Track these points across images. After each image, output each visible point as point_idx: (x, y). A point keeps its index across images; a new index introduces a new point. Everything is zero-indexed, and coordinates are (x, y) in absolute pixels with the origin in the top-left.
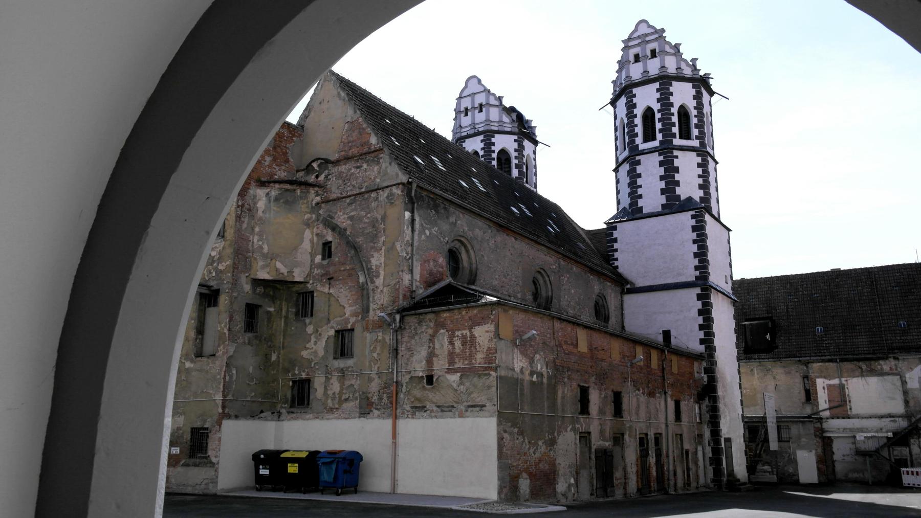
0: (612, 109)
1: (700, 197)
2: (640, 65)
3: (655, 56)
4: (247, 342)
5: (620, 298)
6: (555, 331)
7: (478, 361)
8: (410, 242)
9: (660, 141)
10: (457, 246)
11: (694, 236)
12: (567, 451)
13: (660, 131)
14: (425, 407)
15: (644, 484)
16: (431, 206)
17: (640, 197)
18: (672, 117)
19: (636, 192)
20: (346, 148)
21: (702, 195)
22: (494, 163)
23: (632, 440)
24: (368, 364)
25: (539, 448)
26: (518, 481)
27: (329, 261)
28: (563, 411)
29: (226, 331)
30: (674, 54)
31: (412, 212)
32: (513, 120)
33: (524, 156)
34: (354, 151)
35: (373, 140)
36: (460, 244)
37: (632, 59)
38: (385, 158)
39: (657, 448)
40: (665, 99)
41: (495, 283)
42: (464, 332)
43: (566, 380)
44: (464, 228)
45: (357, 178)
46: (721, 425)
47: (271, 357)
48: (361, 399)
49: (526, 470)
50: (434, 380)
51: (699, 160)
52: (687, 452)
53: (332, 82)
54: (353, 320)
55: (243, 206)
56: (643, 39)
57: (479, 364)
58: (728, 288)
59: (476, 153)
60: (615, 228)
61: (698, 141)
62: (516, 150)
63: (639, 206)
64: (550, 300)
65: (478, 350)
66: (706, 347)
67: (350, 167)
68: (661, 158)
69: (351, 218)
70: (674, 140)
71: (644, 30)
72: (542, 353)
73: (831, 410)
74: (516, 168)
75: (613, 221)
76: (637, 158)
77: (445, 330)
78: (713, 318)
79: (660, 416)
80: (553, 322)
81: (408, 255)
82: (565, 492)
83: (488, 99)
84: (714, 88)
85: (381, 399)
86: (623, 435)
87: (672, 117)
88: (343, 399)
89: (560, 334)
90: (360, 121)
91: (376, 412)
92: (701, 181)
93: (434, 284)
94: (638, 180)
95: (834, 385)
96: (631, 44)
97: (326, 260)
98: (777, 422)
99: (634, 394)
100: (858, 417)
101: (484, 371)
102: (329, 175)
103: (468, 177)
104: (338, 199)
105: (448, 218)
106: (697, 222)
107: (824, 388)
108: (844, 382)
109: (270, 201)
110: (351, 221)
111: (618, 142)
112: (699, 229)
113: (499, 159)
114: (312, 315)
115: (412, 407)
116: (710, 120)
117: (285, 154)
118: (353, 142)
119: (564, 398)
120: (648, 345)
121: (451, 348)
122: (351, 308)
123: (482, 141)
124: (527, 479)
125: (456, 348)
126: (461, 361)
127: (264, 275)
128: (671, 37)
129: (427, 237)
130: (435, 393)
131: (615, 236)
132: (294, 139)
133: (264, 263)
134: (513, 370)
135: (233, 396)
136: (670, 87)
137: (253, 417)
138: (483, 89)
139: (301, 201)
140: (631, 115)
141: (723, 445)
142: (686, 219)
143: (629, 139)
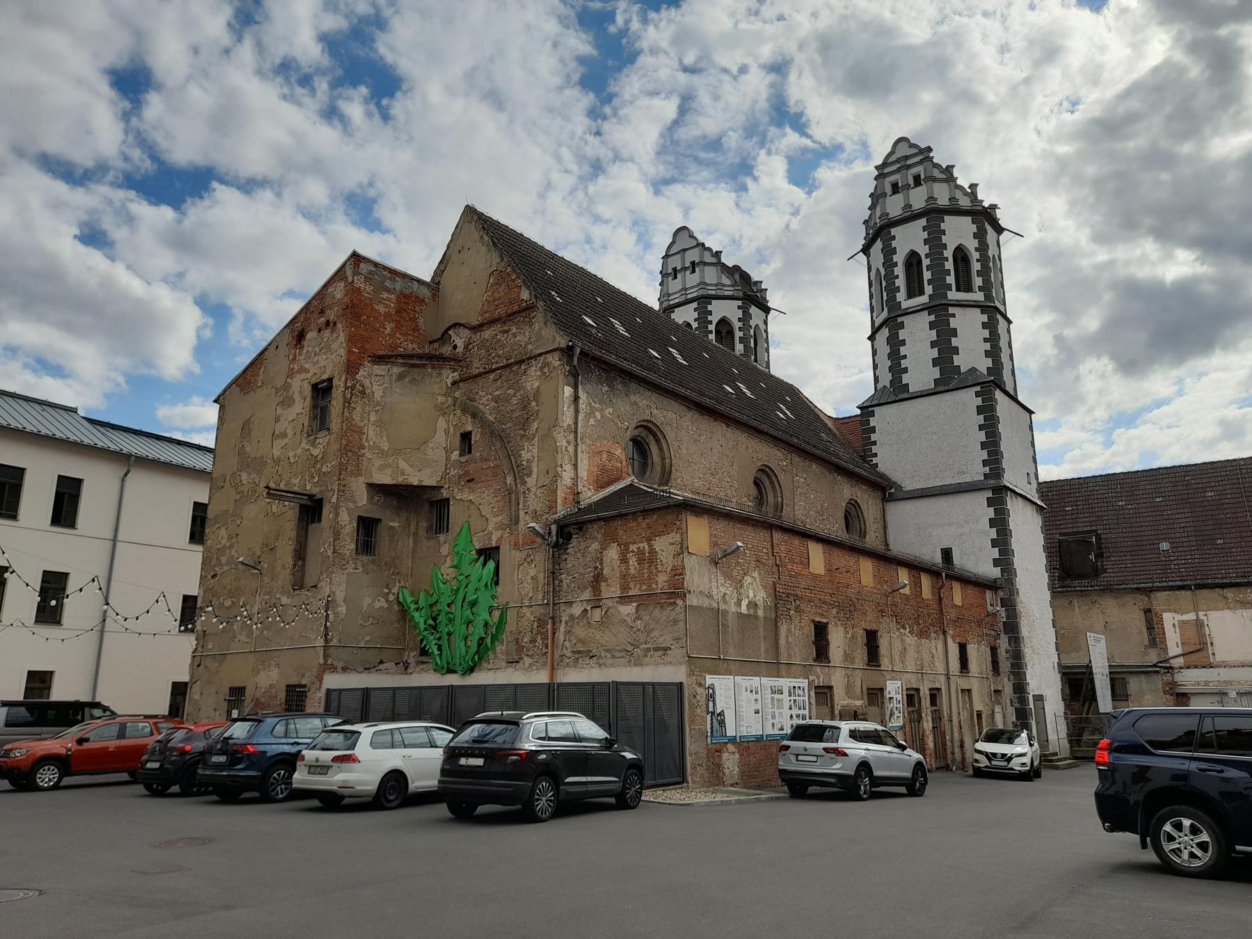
0: (866, 258)
3: (920, 184)
7: (660, 586)
10: (643, 435)
13: (930, 282)
14: (591, 651)
17: (905, 370)
22: (712, 337)
26: (720, 757)
28: (789, 656)
31: (576, 388)
34: (502, 311)
35: (525, 295)
36: (646, 432)
37: (888, 190)
38: (539, 317)
40: (935, 240)
42: (641, 545)
43: (792, 612)
45: (503, 346)
51: (985, 318)
52: (979, 715)
54: (499, 533)
55: (353, 388)
56: (903, 163)
57: (661, 589)
59: (689, 325)
60: (872, 414)
64: (780, 508)
68: (932, 318)
69: (496, 400)
71: (904, 150)
73: (1186, 657)
76: (899, 320)
79: (937, 664)
83: (702, 256)
84: (1002, 223)
91: (527, 661)
92: (988, 346)
93: (609, 484)
94: (902, 348)
95: (1188, 622)
96: (886, 171)
98: (1110, 673)
100: (1224, 665)
101: (668, 599)
103: (662, 346)
104: (480, 375)
107: (1174, 625)
108: (1201, 617)
111: (873, 301)
112: (987, 410)
113: (718, 332)
114: (447, 531)
115: (573, 652)
116: (999, 266)
120: (916, 567)
122: (494, 520)
124: (734, 753)
126: (638, 586)
127: (385, 479)
128: (939, 157)
130: (604, 632)
136: (942, 224)
137: (369, 669)
138: (695, 243)
140: (889, 264)
141: (1032, 706)
142: (969, 399)
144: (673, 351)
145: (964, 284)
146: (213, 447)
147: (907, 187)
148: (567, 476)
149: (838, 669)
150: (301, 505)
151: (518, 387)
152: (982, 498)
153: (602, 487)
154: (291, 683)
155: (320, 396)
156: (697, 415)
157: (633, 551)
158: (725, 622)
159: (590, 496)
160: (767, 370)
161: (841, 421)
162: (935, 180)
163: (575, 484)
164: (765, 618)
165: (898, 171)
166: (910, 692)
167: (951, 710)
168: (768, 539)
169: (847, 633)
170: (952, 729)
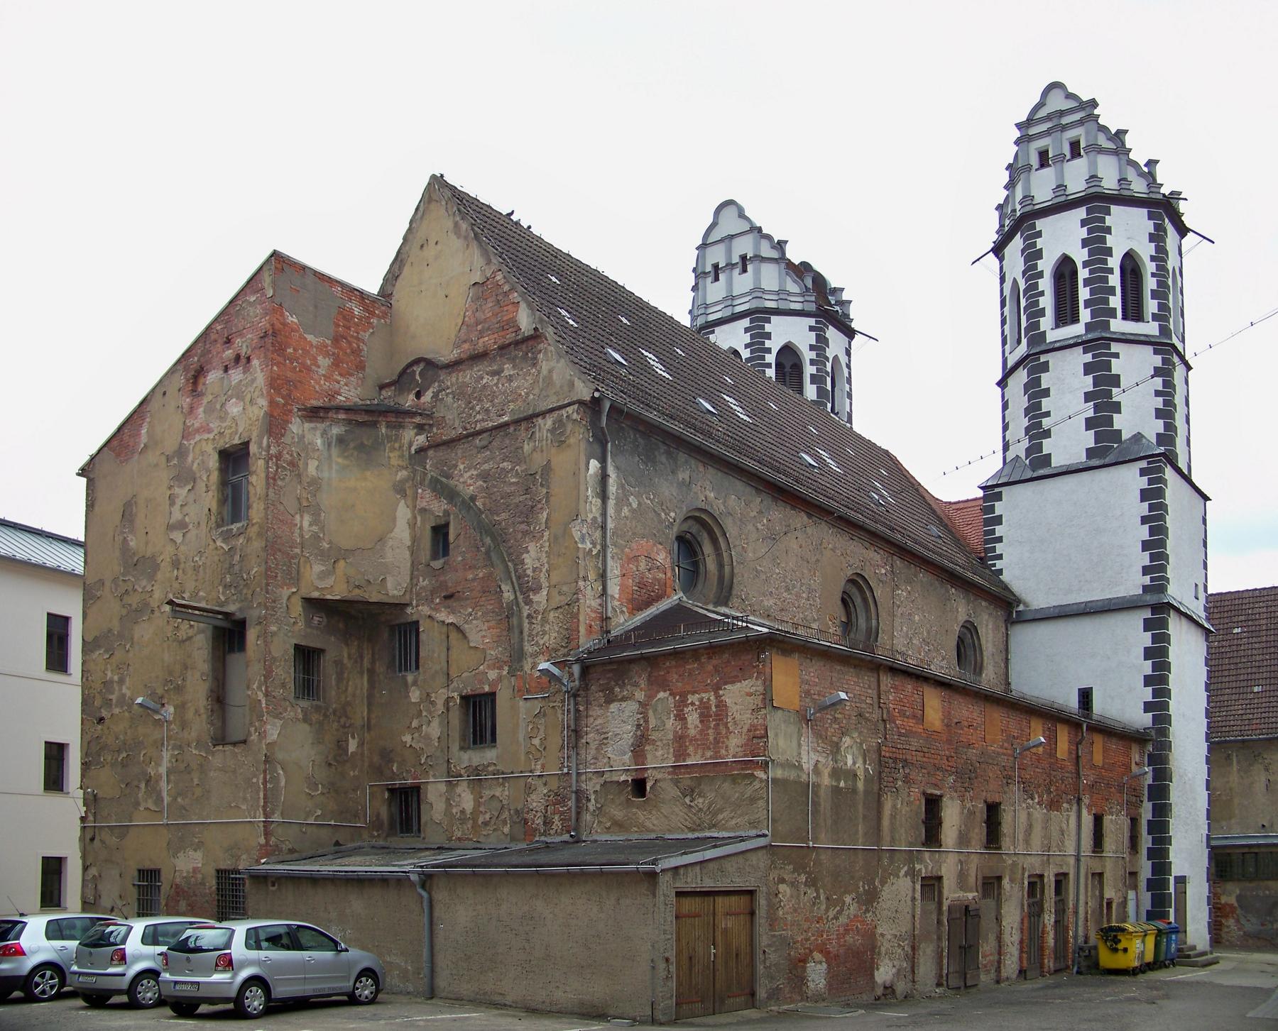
0: (997, 261)
1: (1158, 435)
3: (1079, 155)
4: (301, 716)
6: (882, 692)
7: (732, 751)
8: (599, 520)
9: (1086, 324)
10: (694, 531)
13: (1112, 291)
15: (1032, 962)
16: (640, 449)
22: (771, 373)
23: (1016, 887)
24: (523, 758)
25: (846, 908)
27: (444, 563)
29: (261, 696)
30: (1115, 152)
31: (603, 461)
33: (827, 359)
34: (488, 341)
37: (1034, 160)
39: (1058, 898)
40: (1096, 243)
41: (769, 602)
43: (900, 783)
44: (708, 493)
46: (1171, 855)
50: (648, 788)
51: (1157, 361)
52: (1109, 904)
53: (444, 203)
55: (279, 456)
56: (1055, 122)
57: (734, 756)
58: (1198, 609)
59: (736, 353)
60: (999, 497)
61: (1156, 324)
62: (812, 348)
68: (1088, 358)
69: (485, 476)
70: (1112, 321)
71: (1057, 102)
72: (855, 735)
74: (812, 383)
76: (1043, 358)
77: (668, 692)
78: (1170, 663)
79: (1067, 843)
80: (879, 675)
82: (892, 982)
83: (757, 246)
84: (1187, 221)
85: (547, 823)
86: (999, 878)
88: (480, 823)
89: (891, 698)
90: (498, 278)
92: (1159, 402)
93: (648, 603)
96: (1033, 131)
97: (439, 559)
101: (742, 769)
102: (441, 391)
104: (459, 439)
106: (1150, 482)
109: (329, 445)
110: (485, 482)
111: (1007, 327)
112: (1153, 496)
113: (779, 365)
114: (417, 667)
117: (357, 352)
119: (895, 817)
120: (1051, 716)
123: (747, 330)
124: (821, 963)
126: (700, 752)
127: (336, 590)
128: (1109, 117)
129: (633, 511)
132: (374, 321)
133: (324, 568)
134: (800, 767)
135: (282, 814)
136: (1107, 217)
140: (1032, 274)
141: (1172, 890)
142: (1131, 479)
144: (731, 400)
145: (1133, 311)
146: (83, 540)
147: (1061, 158)
148: (589, 601)
149: (950, 854)
150: (216, 628)
151: (516, 456)
152: (1136, 620)
153: (640, 609)
154: (223, 867)
155: (231, 470)
156: (768, 501)
157: (692, 704)
158: (816, 799)
159: (623, 622)
160: (848, 425)
161: (954, 507)
162: (1101, 151)
163: (604, 605)
164: (866, 792)
165: (1048, 133)
166: (1032, 880)
167: (1078, 900)
168: (874, 685)
169: (963, 807)
170: (1077, 924)
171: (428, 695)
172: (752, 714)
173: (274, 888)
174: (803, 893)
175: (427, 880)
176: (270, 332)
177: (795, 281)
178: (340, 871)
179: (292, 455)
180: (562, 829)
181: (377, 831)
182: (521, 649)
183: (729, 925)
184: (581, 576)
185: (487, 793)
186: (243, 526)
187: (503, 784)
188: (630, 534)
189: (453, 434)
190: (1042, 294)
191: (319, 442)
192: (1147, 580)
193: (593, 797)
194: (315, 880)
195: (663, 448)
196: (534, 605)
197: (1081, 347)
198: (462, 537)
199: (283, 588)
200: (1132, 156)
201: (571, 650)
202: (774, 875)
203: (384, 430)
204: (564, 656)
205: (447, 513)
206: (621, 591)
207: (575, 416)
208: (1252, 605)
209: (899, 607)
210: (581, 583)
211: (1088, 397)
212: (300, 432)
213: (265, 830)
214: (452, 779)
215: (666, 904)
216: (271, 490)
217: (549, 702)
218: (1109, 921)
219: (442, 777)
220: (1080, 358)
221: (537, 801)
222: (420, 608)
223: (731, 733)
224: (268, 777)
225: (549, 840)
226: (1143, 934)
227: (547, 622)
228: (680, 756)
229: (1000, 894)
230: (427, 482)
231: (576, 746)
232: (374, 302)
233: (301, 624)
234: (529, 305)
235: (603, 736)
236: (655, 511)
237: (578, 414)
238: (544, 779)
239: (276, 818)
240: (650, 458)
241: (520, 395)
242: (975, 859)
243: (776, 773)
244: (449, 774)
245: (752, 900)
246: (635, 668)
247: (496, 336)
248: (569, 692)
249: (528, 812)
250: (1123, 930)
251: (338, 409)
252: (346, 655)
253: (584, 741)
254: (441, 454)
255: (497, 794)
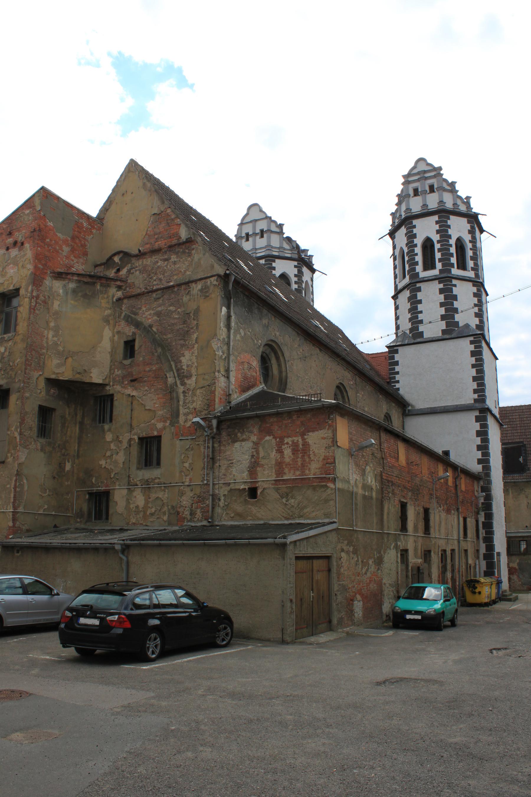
1: (476, 325)
2: (418, 199)
4: (39, 448)
5: (401, 419)
7: (312, 472)
8: (226, 340)
10: (267, 352)
11: (473, 360)
12: (390, 570)
13: (452, 255)
18: (451, 248)
19: (417, 317)
20: (152, 241)
21: (478, 323)
25: (370, 568)
29: (17, 435)
31: (228, 308)
32: (293, 246)
33: (303, 282)
34: (161, 243)
37: (411, 193)
42: (295, 439)
43: (390, 494)
44: (276, 332)
46: (495, 540)
47: (65, 466)
48: (170, 514)
49: (360, 592)
50: (259, 493)
53: (137, 173)
55: (37, 297)
56: (422, 175)
57: (314, 474)
60: (397, 352)
61: (473, 272)
62: (296, 276)
63: (420, 331)
65: (312, 458)
66: (483, 467)
67: (156, 260)
68: (441, 286)
69: (158, 314)
70: (452, 269)
71: (422, 167)
75: (394, 344)
76: (418, 285)
77: (272, 437)
78: (489, 439)
80: (380, 433)
81: (223, 354)
83: (269, 226)
85: (192, 514)
87: (451, 248)
88: (148, 513)
94: (419, 306)
96: (411, 179)
99: (438, 510)
101: (320, 482)
105: (261, 319)
106: (475, 347)
109: (67, 293)
110: (158, 317)
114: (111, 420)
117: (84, 246)
118: (160, 233)
121: (279, 457)
125: (285, 456)
126: (292, 472)
128: (448, 175)
129: (242, 337)
131: (396, 359)
132: (94, 231)
133: (59, 362)
134: (348, 482)
138: (264, 216)
139: (101, 295)
140: (411, 245)
141: (496, 560)
143: (409, 267)
145: (462, 265)
147: (424, 192)
148: (222, 382)
157: (287, 443)
159: (237, 398)
161: (371, 356)
162: (445, 190)
164: (377, 499)
169: (415, 510)
171: (118, 437)
172: (325, 449)
173: (18, 554)
174: (351, 558)
175: (126, 548)
176: (37, 229)
177: (287, 243)
178: (65, 543)
179: (45, 297)
180: (202, 518)
181: (80, 518)
182: (178, 411)
183: (319, 578)
184: (217, 370)
185: (153, 496)
186: (12, 335)
187: (164, 491)
188: (240, 349)
189: (139, 291)
190: (417, 254)
191: (61, 291)
192: (476, 396)
193: (222, 498)
194: (47, 549)
195: (256, 305)
196: (188, 386)
197: (437, 281)
198: (143, 347)
199: (34, 372)
200: (458, 194)
201: (210, 411)
202: (339, 547)
203: (99, 287)
204: (206, 415)
205: (134, 334)
206: (236, 381)
207: (215, 283)
208: (511, 414)
209: (359, 402)
210: (217, 374)
211: (442, 305)
212: (50, 285)
213: (13, 518)
214: (131, 486)
215: (290, 565)
216: (32, 315)
217: (196, 441)
218: (471, 577)
219: (124, 485)
220: (437, 286)
221: (186, 501)
222: (115, 387)
223: (312, 461)
224: (18, 484)
225: (193, 524)
226: (490, 583)
227: (195, 395)
228: (279, 474)
229: (430, 560)
230: (122, 317)
231: (213, 468)
232: (94, 221)
233: (44, 393)
234: (187, 226)
235: (230, 462)
236: (252, 339)
237: (217, 281)
238: (191, 487)
239: (21, 509)
240: (250, 311)
241: (181, 271)
242: (420, 539)
243: (339, 485)
244: (129, 484)
245: (329, 562)
246: (251, 422)
247: (166, 241)
248: (208, 436)
249: (180, 508)
250: (478, 582)
251: (73, 274)
252: (67, 413)
253: (217, 464)
254: (132, 301)
255: (160, 496)
